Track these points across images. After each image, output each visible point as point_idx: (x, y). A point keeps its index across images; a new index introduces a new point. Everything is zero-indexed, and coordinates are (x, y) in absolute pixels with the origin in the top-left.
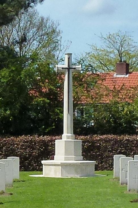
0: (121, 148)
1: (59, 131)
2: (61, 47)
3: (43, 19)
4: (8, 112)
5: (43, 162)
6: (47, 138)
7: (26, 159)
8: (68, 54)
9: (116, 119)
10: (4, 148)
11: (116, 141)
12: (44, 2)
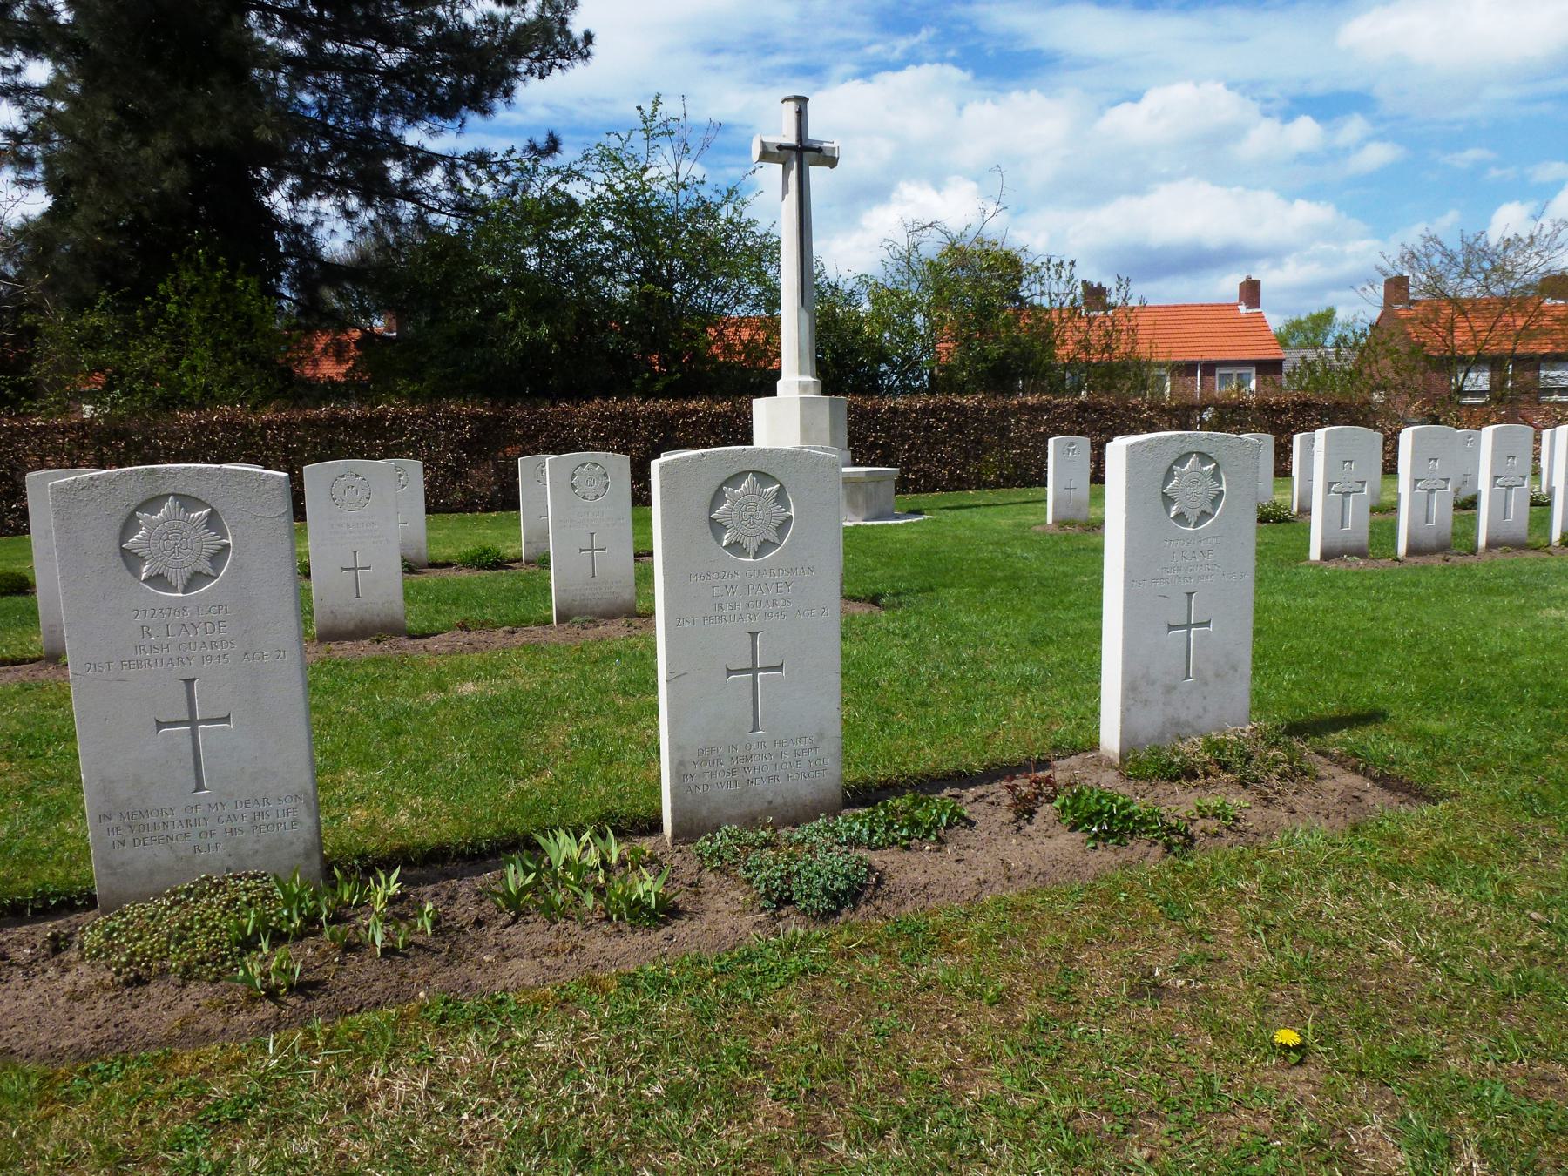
0: (876, 431)
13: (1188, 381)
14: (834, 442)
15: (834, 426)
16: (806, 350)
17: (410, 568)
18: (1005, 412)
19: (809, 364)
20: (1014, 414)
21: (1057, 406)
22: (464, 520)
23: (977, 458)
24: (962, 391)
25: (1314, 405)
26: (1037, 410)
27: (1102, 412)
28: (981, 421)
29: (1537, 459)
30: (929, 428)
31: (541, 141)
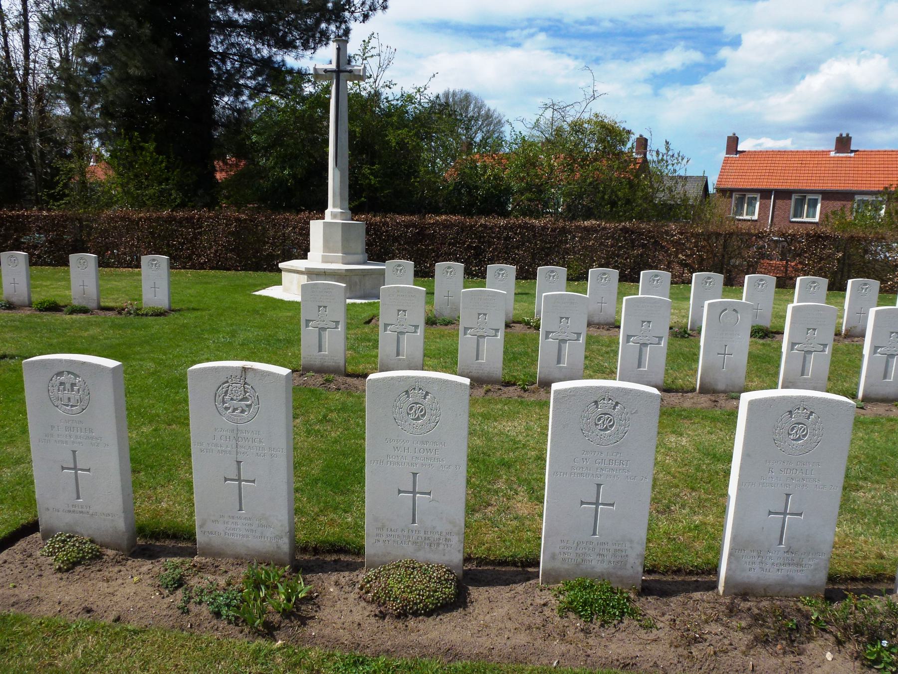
0: (472, 239)
1: (320, 207)
2: (599, 207)
3: (489, 110)
4: (286, 172)
9: (472, 189)
11: (463, 228)
16: (341, 188)
20: (570, 233)
21: (604, 229)
22: (122, 274)
25: (827, 237)
30: (507, 238)
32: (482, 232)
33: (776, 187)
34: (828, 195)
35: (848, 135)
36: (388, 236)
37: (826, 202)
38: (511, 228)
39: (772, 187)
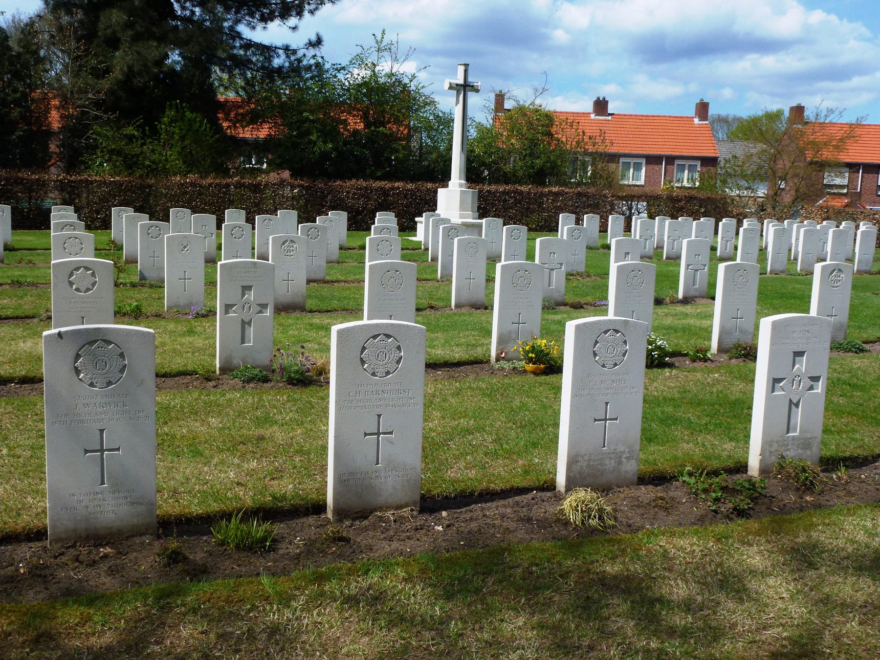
1: (444, 178)
2: (537, 174)
5: (389, 221)
6: (430, 185)
7: (358, 213)
8: (465, 65)
10: (329, 197)
12: (338, 5)
13: (656, 167)
14: (462, 207)
15: (473, 203)
17: (341, 248)
18: (542, 195)
19: (463, 176)
20: (546, 196)
21: (567, 193)
23: (527, 216)
24: (520, 182)
25: (696, 198)
26: (557, 194)
27: (588, 197)
28: (530, 199)
29: (762, 231)
30: (505, 201)
31: (314, 38)
32: (488, 196)
33: (666, 153)
34: (653, 160)
35: (604, 99)
36: (421, 200)
37: (651, 167)
38: (508, 193)
39: (663, 153)
